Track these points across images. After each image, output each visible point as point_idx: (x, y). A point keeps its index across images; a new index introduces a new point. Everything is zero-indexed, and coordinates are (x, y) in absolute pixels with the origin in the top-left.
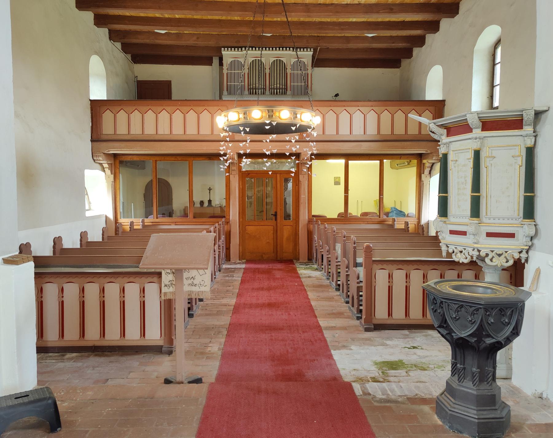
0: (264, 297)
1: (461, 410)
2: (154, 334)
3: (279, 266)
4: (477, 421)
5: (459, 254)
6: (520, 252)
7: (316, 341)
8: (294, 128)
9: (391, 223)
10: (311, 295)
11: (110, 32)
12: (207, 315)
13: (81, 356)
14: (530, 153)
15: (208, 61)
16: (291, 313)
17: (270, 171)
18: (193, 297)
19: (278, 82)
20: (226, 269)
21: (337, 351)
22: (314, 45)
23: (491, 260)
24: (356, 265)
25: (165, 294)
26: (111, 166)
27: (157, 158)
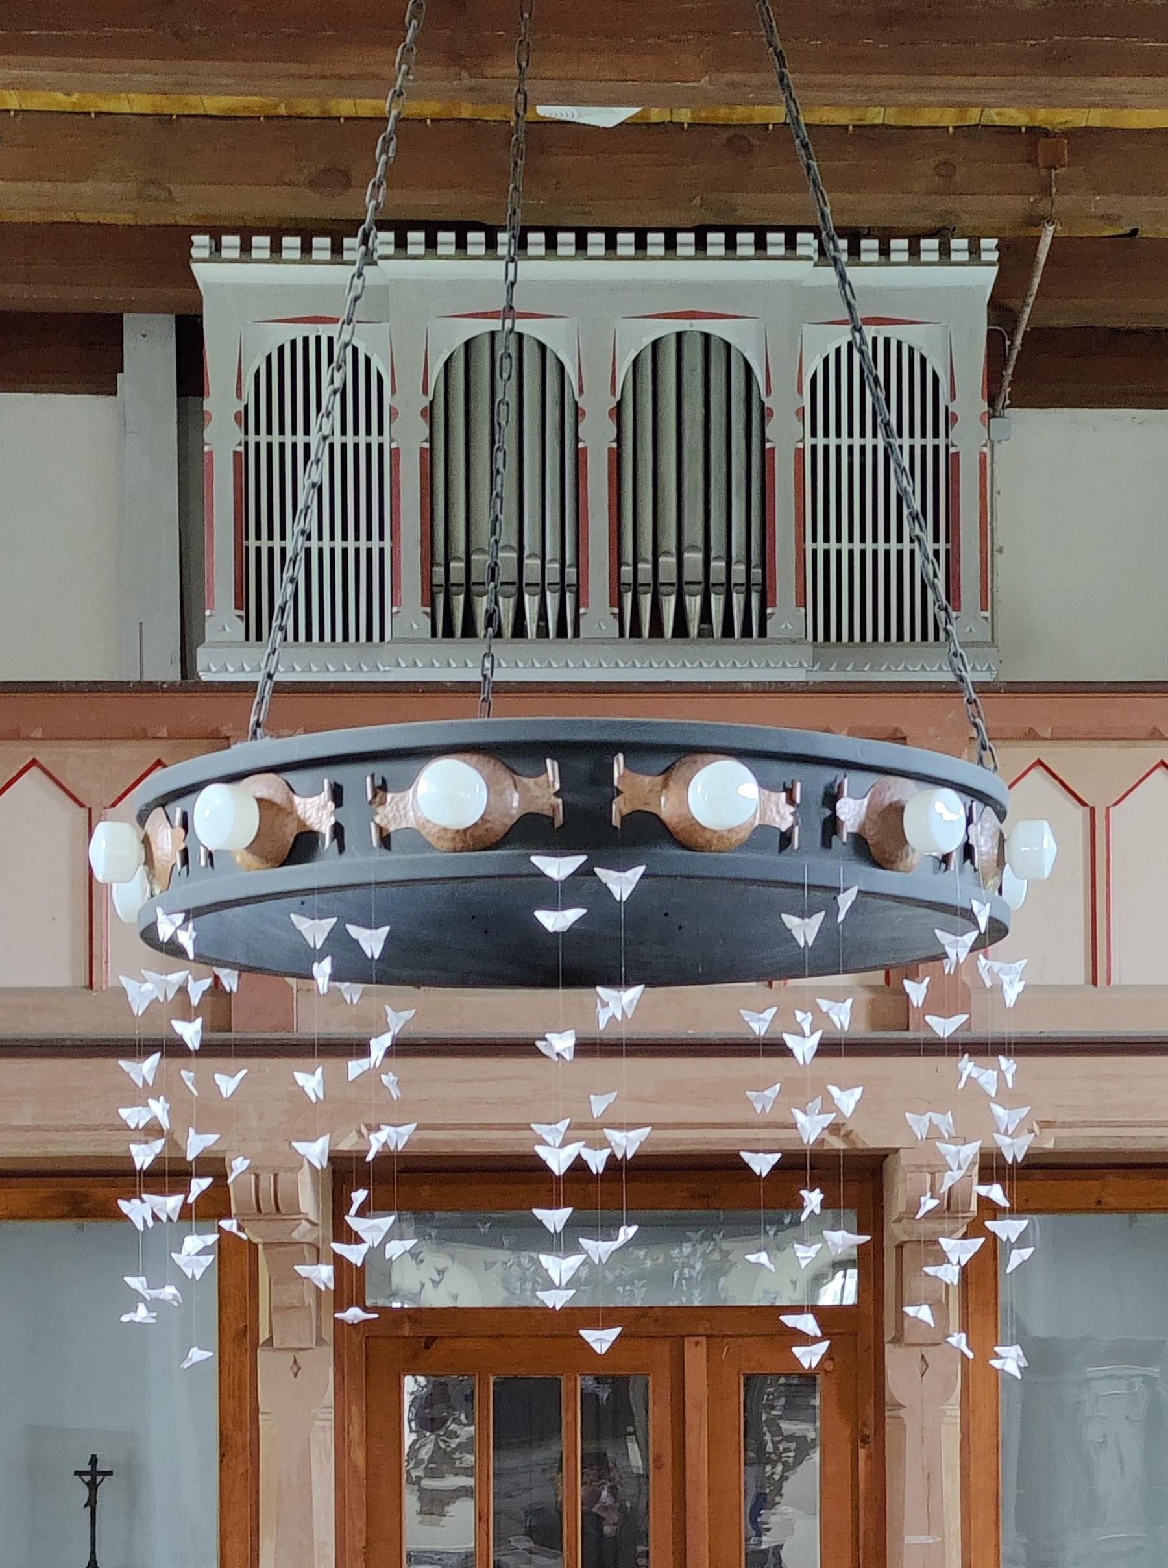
8: (804, 930)
17: (600, 1318)
19: (694, 533)
22: (1016, 204)
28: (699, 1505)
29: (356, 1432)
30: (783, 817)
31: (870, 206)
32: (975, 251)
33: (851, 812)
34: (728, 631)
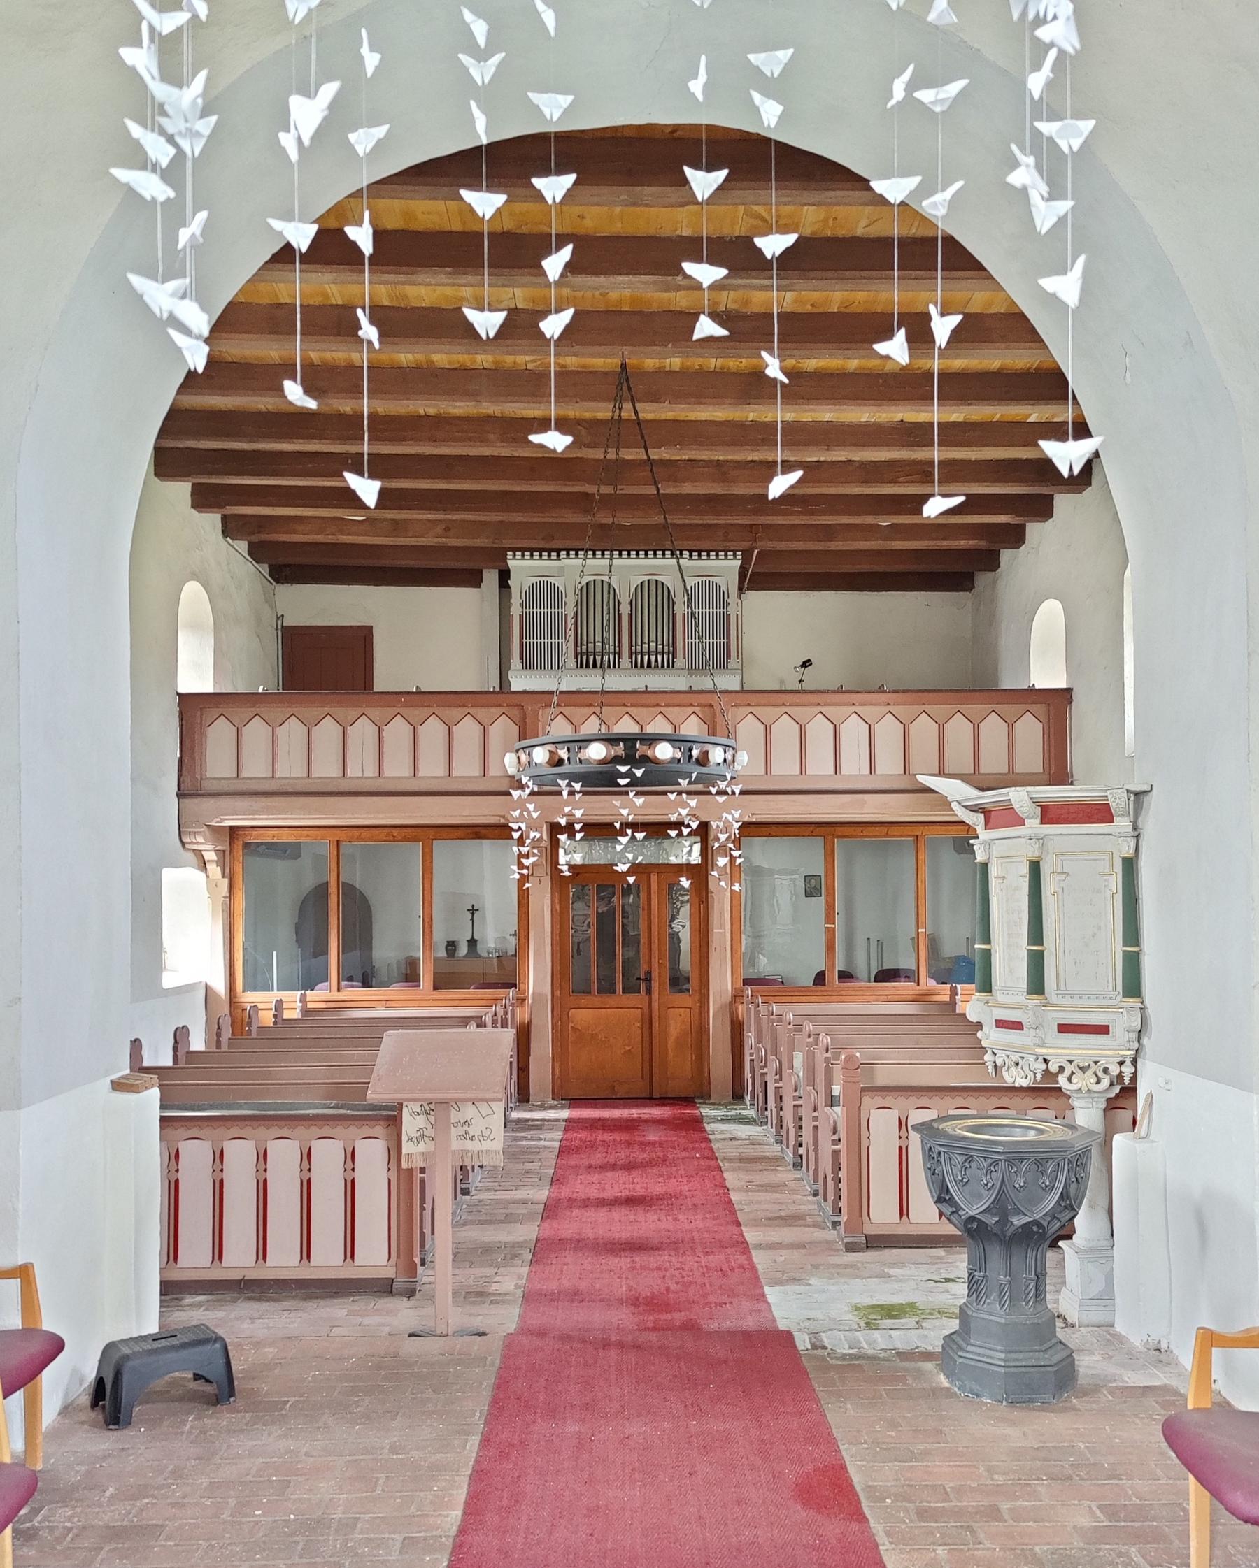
0: (617, 1184)
1: (979, 1355)
2: (374, 1256)
3: (656, 1112)
4: (1003, 1370)
5: (1013, 1069)
6: (1121, 1063)
7: (732, 1270)
9: (947, 999)
10: (731, 1178)
11: (225, 519)
12: (481, 1222)
13: (219, 1301)
14: (1130, 866)
15: (473, 579)
16: (681, 1217)
18: (468, 1162)
19: (653, 637)
20: (519, 1121)
21: (778, 1288)
22: (746, 545)
23: (1070, 1080)
24: (832, 1101)
25: (409, 1156)
26: (224, 859)
27: (341, 835)
28: (655, 921)
29: (557, 900)
30: (678, 755)
31: (705, 545)
32: (735, 555)
33: (695, 753)
34: (663, 666)
